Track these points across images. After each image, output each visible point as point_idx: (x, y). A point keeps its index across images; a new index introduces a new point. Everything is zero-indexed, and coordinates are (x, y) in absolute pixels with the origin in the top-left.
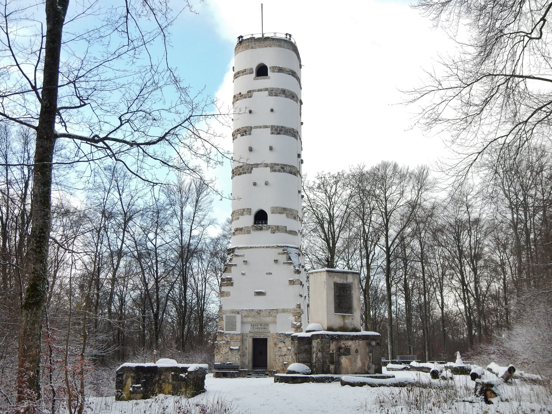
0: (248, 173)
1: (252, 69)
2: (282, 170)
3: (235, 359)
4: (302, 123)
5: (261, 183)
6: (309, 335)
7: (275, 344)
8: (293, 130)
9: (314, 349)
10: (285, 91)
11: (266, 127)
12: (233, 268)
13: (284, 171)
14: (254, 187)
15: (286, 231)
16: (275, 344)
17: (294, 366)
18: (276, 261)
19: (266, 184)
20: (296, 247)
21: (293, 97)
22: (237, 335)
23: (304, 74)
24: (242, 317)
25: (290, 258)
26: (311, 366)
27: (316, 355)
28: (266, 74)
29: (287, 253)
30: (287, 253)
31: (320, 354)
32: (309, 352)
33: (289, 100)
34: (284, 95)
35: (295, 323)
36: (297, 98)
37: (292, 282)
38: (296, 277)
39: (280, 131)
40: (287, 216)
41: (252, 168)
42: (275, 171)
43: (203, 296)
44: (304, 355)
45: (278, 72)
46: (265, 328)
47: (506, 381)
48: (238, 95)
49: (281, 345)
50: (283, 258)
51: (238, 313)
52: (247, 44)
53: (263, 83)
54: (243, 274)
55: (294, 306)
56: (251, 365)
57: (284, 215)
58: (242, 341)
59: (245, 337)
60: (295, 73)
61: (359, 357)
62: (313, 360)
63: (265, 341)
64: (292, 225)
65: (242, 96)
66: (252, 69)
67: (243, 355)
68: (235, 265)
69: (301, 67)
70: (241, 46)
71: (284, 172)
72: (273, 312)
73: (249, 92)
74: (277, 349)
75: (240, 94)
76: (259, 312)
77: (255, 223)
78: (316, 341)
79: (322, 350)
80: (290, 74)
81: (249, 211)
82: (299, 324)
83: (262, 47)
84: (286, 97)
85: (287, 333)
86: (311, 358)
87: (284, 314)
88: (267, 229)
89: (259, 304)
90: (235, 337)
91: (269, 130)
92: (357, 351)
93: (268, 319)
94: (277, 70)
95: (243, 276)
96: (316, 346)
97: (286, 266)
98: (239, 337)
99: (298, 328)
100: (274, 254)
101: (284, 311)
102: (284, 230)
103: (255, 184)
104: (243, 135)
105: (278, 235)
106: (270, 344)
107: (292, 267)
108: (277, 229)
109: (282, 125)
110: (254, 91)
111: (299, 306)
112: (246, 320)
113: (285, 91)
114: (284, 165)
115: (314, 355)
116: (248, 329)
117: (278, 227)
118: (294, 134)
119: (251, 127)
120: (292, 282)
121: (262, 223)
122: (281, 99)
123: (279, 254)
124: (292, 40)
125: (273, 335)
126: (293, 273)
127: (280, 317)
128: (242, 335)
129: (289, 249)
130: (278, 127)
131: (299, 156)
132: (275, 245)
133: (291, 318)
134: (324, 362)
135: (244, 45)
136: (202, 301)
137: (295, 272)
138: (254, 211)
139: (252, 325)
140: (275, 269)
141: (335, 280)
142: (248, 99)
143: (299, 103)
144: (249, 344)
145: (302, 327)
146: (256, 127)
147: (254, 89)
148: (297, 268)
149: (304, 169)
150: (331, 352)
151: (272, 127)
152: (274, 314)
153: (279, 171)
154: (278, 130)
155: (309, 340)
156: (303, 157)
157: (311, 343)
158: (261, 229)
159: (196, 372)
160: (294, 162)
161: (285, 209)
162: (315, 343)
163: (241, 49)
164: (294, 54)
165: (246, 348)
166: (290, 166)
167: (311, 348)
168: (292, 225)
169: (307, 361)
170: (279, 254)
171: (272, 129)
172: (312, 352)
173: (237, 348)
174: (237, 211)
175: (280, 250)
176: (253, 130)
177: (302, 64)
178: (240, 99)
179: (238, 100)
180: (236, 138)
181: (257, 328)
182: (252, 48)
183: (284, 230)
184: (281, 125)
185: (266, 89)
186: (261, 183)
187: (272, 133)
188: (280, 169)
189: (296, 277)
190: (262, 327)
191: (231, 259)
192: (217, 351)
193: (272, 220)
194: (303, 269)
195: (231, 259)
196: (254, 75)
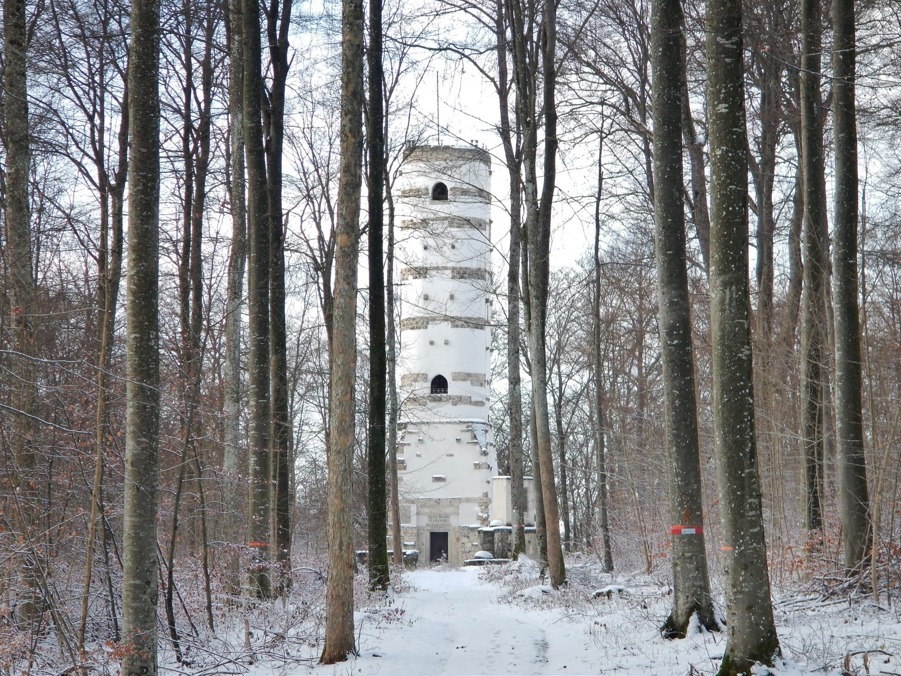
5: (440, 342)
6: (492, 529)
7: (458, 539)
9: (496, 540)
12: (405, 448)
14: (431, 346)
15: (471, 403)
16: (458, 539)
17: (480, 553)
18: (458, 440)
19: (446, 343)
20: (483, 421)
22: (412, 528)
24: (418, 507)
25: (475, 437)
26: (493, 554)
27: (497, 545)
29: (472, 431)
30: (472, 431)
31: (500, 544)
32: (492, 542)
35: (481, 514)
37: (478, 466)
38: (483, 459)
40: (472, 384)
41: (428, 323)
42: (457, 326)
44: (488, 545)
49: (465, 540)
50: (467, 437)
51: (413, 503)
53: (442, 208)
54: (419, 456)
55: (479, 494)
57: (469, 382)
58: (418, 535)
59: (421, 531)
63: (445, 535)
64: (477, 392)
66: (427, 189)
68: (409, 444)
72: (455, 502)
74: (460, 545)
76: (438, 501)
77: (432, 392)
79: (502, 541)
81: (425, 377)
82: (485, 515)
85: (471, 526)
86: (493, 546)
87: (468, 504)
88: (447, 400)
90: (410, 531)
91: (449, 273)
92: (529, 542)
93: (449, 510)
95: (418, 458)
97: (469, 445)
98: (415, 531)
99: (485, 521)
100: (455, 431)
101: (468, 500)
102: (469, 401)
103: (432, 343)
105: (462, 408)
106: (451, 539)
107: (478, 447)
108: (458, 400)
111: (486, 495)
114: (468, 318)
116: (424, 521)
117: (461, 397)
119: (426, 268)
120: (478, 466)
121: (441, 392)
123: (462, 431)
124: (480, 146)
125: (454, 528)
126: (479, 454)
127: (463, 507)
128: (418, 528)
129: (474, 425)
132: (457, 420)
133: (477, 509)
134: (503, 550)
135: (418, 153)
137: (481, 454)
138: (431, 376)
139: (430, 517)
140: (457, 449)
144: (426, 540)
148: (484, 449)
152: (456, 504)
153: (462, 326)
154: (461, 274)
155: (492, 534)
158: (440, 400)
159: (412, 554)
161: (469, 375)
162: (496, 536)
167: (493, 539)
168: (477, 392)
169: (491, 550)
170: (462, 431)
171: (453, 272)
173: (413, 543)
175: (464, 427)
183: (469, 401)
186: (440, 342)
187: (453, 278)
189: (483, 459)
191: (403, 438)
192: (709, 492)
193: (453, 388)
195: (403, 438)
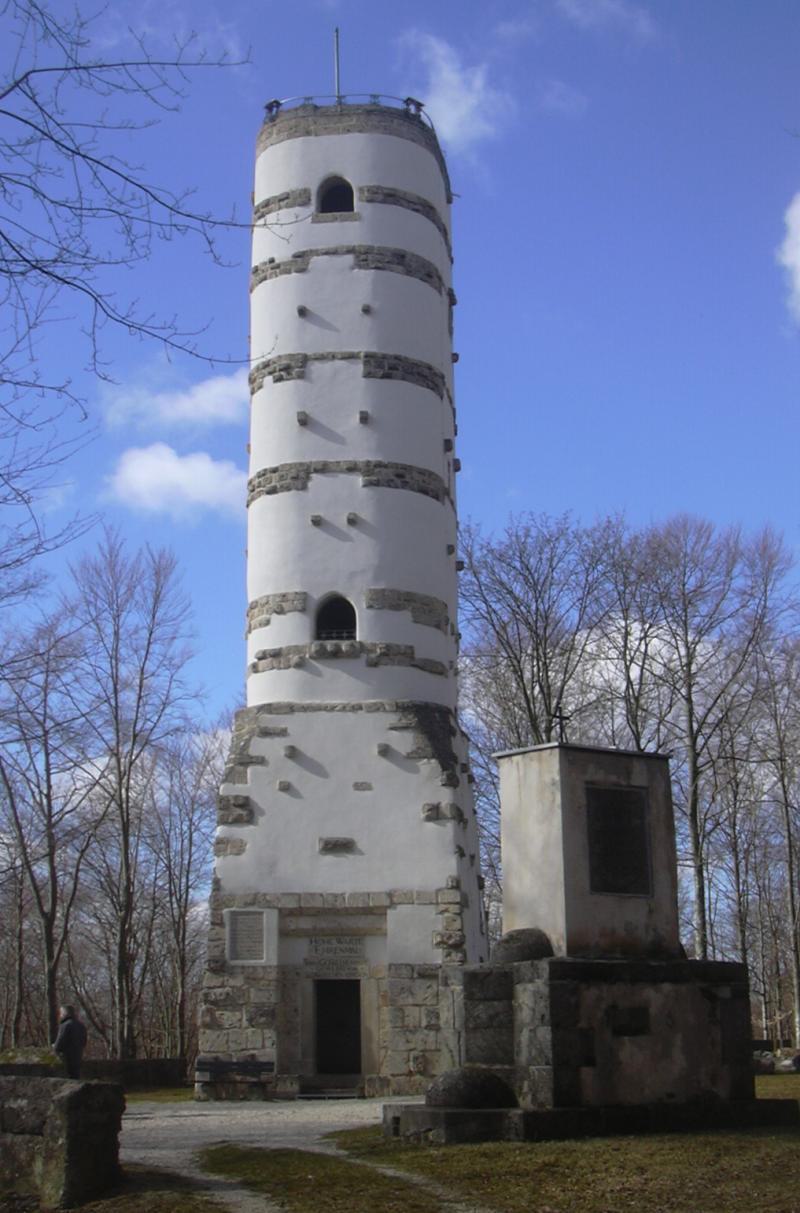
0: (298, 489)
1: (306, 192)
2: (398, 481)
3: (263, 1045)
4: (455, 358)
8: (430, 368)
10: (403, 257)
11: (351, 357)
13: (405, 485)
21: (429, 276)
23: (457, 217)
28: (348, 206)
33: (414, 283)
34: (400, 268)
36: (440, 279)
39: (390, 368)
43: (185, 867)
45: (383, 202)
46: (351, 950)
47: (248, 978)
48: (265, 264)
52: (293, 122)
56: (310, 1060)
60: (432, 208)
61: (678, 1040)
62: (518, 1053)
63: (352, 988)
65: (278, 266)
67: (285, 1033)
69: (449, 201)
70: (275, 130)
71: (403, 488)
73: (298, 256)
75: (272, 261)
78: (530, 986)
80: (417, 211)
83: (336, 131)
84: (409, 273)
89: (336, 879)
91: (359, 368)
94: (381, 197)
96: (531, 1005)
104: (279, 379)
109: (398, 353)
110: (316, 253)
112: (293, 927)
113: (403, 257)
114: (405, 467)
115: (524, 1037)
118: (431, 379)
122: (396, 278)
130: (384, 357)
131: (448, 445)
136: (184, 880)
141: (588, 777)
142: (294, 274)
143: (446, 299)
144: (305, 997)
145: (465, 946)
146: (322, 358)
147: (313, 248)
149: (464, 485)
150: (583, 1024)
151: (369, 357)
156: (459, 452)
157: (509, 995)
160: (436, 464)
163: (274, 136)
164: (431, 227)
165: (296, 1010)
166: (422, 472)
167: (511, 1011)
171: (366, 363)
172: (517, 1023)
174: (264, 601)
176: (309, 363)
177: (453, 190)
178: (271, 278)
179: (265, 279)
180: (260, 387)
181: (329, 951)
182: (308, 133)
184: (391, 351)
185: (350, 251)
188: (393, 477)
190: (341, 946)
194: (465, 775)
196: (312, 208)
